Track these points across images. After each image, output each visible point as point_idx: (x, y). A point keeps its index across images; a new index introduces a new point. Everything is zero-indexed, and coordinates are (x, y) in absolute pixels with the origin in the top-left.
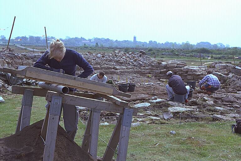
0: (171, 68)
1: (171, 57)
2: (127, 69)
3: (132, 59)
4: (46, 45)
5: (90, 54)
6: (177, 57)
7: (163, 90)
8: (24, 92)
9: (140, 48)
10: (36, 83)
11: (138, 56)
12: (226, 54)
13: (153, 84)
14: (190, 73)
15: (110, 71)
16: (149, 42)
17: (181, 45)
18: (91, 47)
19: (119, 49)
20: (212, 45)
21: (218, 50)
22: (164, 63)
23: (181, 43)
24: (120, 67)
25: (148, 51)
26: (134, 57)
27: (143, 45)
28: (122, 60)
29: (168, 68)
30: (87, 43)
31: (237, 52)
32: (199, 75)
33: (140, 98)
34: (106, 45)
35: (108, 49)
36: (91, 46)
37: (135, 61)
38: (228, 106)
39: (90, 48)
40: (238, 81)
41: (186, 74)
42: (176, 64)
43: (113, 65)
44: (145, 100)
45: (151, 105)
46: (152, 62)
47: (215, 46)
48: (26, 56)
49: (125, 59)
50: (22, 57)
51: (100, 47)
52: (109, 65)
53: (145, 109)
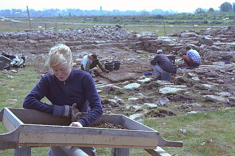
0: (145, 40)
1: (133, 24)
2: (106, 43)
3: (110, 33)
4: (28, 16)
5: (71, 30)
6: (138, 23)
7: (146, 65)
8: (19, 136)
9: (106, 16)
10: (23, 65)
11: (115, 30)
12: (177, 19)
13: (135, 59)
14: (164, 44)
15: (91, 46)
16: (113, 10)
17: (139, 12)
18: (65, 17)
19: (88, 18)
20: (164, 12)
21: (170, 16)
22: (139, 36)
23: (139, 11)
24: (100, 41)
25: (113, 19)
26: (111, 31)
27: (108, 13)
28: (101, 35)
29: (143, 40)
30: (61, 14)
31: (186, 17)
32: (173, 46)
33: (128, 78)
34: (78, 15)
35: (79, 18)
36: (65, 16)
37: (113, 35)
38: (213, 82)
39: (64, 18)
40: (210, 52)
41: (160, 46)
42: (149, 36)
43: (93, 40)
44: (133, 80)
45: (141, 86)
46: (128, 35)
47: (167, 12)
48: (12, 36)
49: (104, 33)
50: (7, 37)
51: (72, 16)
52: (90, 40)
53: (137, 90)
